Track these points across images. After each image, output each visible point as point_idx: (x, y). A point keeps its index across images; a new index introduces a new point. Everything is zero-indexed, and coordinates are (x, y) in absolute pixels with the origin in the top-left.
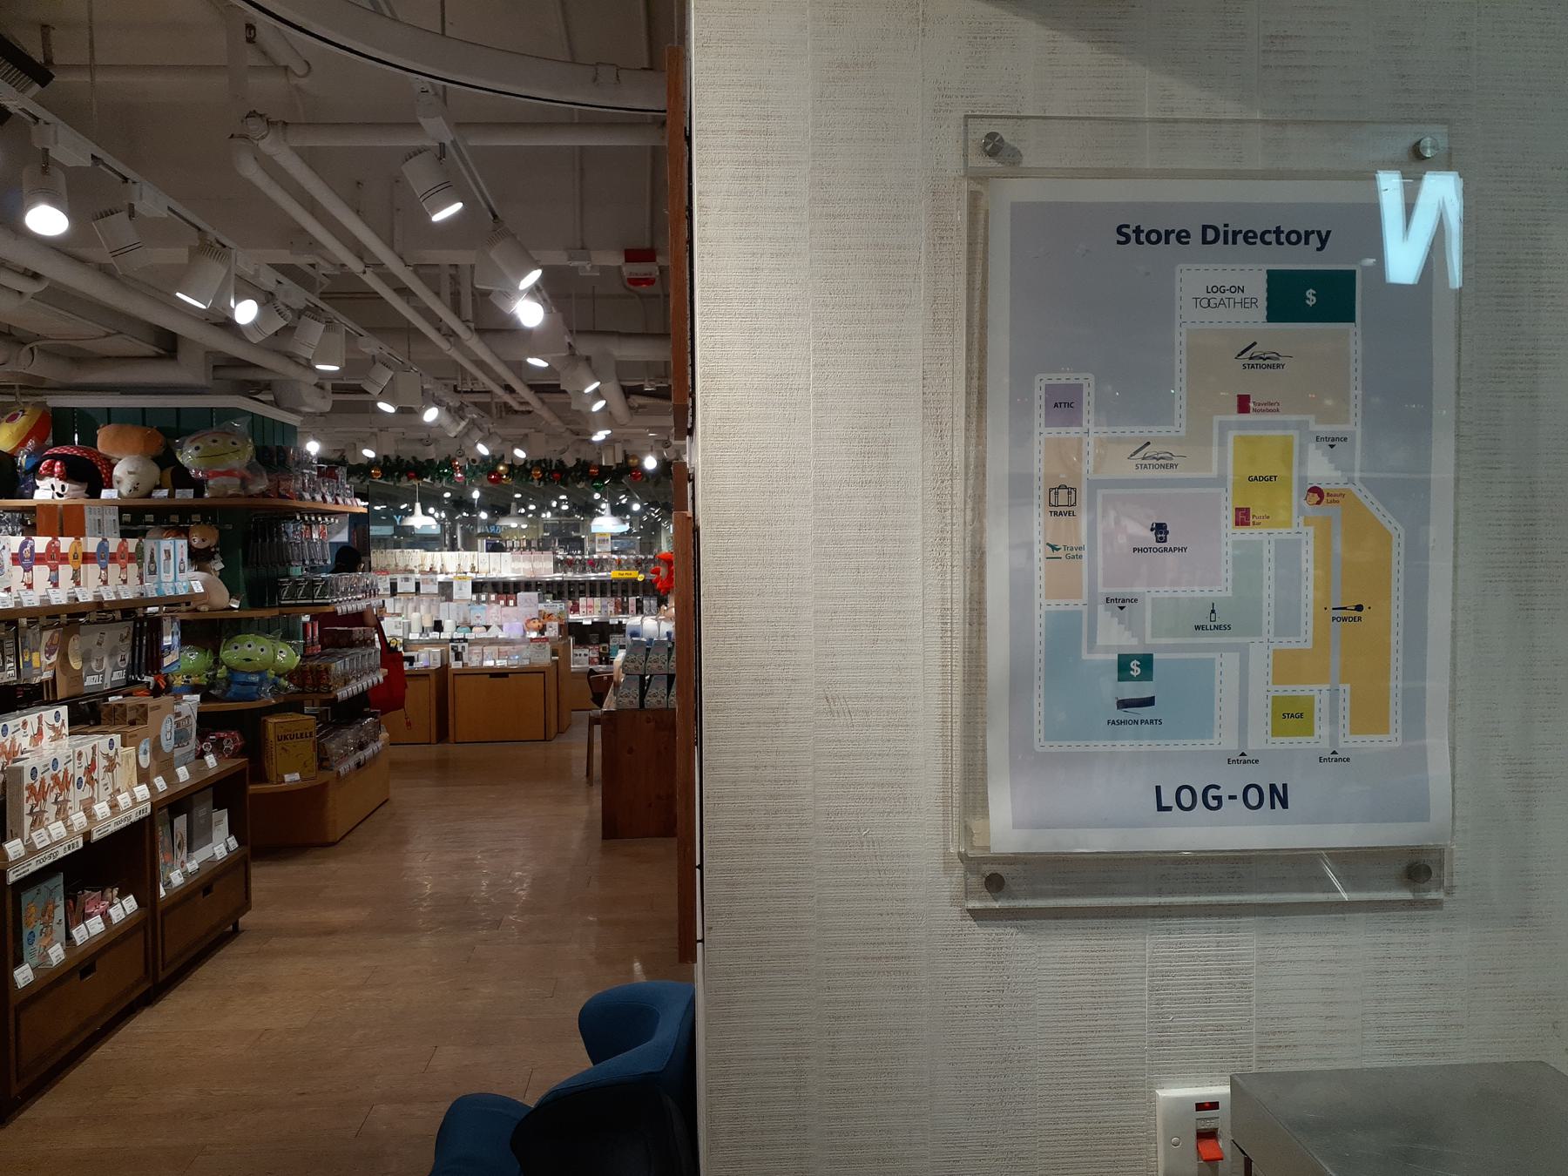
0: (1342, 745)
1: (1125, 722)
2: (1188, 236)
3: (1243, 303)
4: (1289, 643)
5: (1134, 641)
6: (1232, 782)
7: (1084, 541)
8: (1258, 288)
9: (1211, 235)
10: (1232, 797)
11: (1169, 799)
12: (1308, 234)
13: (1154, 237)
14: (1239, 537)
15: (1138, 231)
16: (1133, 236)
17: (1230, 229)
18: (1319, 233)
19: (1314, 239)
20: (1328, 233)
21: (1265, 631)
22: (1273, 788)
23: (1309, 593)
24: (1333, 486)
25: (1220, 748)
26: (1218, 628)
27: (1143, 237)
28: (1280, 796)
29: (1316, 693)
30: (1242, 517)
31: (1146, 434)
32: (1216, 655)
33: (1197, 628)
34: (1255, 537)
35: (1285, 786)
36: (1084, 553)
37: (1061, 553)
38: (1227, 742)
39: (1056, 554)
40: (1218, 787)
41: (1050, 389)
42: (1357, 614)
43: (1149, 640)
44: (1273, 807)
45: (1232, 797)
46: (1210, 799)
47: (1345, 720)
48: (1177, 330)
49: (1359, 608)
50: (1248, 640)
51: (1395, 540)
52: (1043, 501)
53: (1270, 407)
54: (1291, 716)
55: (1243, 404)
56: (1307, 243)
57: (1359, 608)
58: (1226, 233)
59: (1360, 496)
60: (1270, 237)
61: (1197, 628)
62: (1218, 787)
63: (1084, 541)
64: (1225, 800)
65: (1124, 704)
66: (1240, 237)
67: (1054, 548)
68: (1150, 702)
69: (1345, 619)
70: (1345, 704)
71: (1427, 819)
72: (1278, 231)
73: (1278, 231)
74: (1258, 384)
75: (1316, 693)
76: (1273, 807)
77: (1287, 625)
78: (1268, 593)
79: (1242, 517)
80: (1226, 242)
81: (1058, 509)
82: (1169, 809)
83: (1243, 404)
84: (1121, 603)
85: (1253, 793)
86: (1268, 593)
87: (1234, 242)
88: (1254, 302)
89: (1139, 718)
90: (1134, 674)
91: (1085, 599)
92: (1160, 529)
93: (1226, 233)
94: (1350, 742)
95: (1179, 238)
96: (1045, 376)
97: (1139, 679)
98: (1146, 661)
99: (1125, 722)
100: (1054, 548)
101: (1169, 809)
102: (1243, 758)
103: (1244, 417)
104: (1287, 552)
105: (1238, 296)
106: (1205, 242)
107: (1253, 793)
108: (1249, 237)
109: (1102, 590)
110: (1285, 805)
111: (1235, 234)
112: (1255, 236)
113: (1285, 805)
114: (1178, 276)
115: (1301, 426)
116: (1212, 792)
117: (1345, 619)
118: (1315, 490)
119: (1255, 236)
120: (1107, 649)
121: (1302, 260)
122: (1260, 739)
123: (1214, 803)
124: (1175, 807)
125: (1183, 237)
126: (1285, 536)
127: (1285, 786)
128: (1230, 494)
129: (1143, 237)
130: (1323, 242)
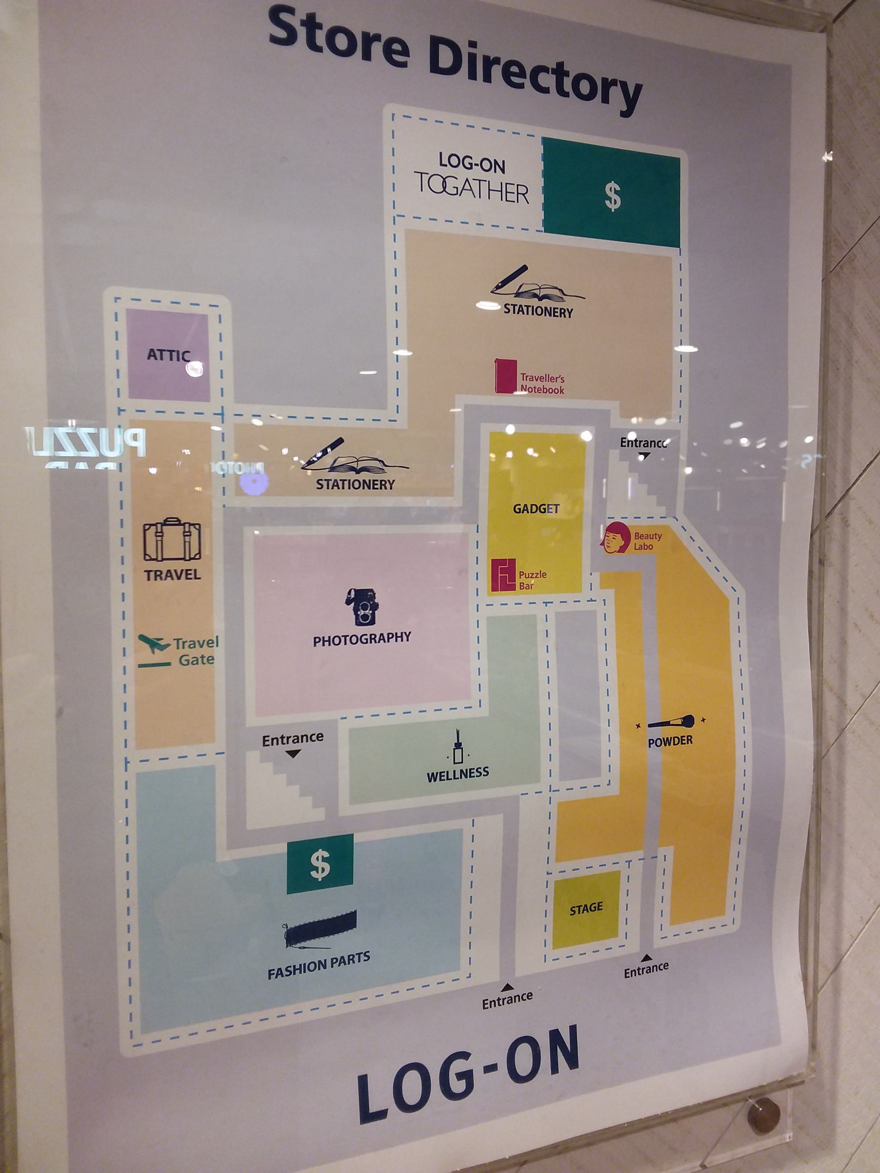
0: (658, 943)
1: (303, 968)
2: (405, 52)
3: (504, 192)
4: (582, 789)
5: (319, 815)
6: (488, 1042)
7: (219, 627)
8: (528, 169)
9: (446, 58)
10: (491, 1068)
11: (381, 1097)
12: (607, 84)
13: (342, 42)
14: (497, 611)
15: (311, 23)
16: (302, 32)
17: (480, 52)
18: (624, 85)
19: (616, 93)
20: (638, 88)
21: (544, 772)
22: (555, 1036)
23: (609, 704)
24: (644, 522)
25: (471, 983)
26: (467, 774)
27: (321, 38)
28: (565, 1048)
29: (622, 866)
30: (504, 575)
31: (335, 423)
32: (464, 824)
33: (432, 777)
34: (525, 610)
35: (573, 1029)
36: (219, 653)
37: (170, 654)
38: (482, 968)
39: (159, 656)
40: (465, 1055)
41: (137, 318)
42: (684, 731)
43: (347, 809)
44: (555, 1069)
45: (491, 1068)
46: (452, 1080)
47: (663, 905)
48: (389, 229)
49: (688, 721)
50: (516, 790)
51: (733, 608)
52: (131, 551)
53: (548, 385)
54: (585, 907)
55: (506, 376)
56: (605, 100)
57: (688, 721)
58: (472, 58)
59: (684, 538)
60: (547, 80)
61: (432, 777)
62: (465, 1055)
63: (219, 627)
64: (479, 1077)
65: (297, 935)
66: (497, 71)
67: (154, 644)
68: (347, 922)
69: (667, 742)
70: (664, 881)
71: (778, 1042)
72: (560, 71)
73: (560, 71)
74: (533, 343)
75: (622, 867)
76: (555, 1069)
77: (580, 763)
78: (549, 704)
79: (504, 575)
80: (472, 76)
81: (164, 566)
82: (382, 1114)
83: (506, 376)
84: (291, 744)
85: (524, 1053)
86: (549, 704)
87: (487, 78)
88: (523, 193)
89: (327, 956)
90: (319, 876)
91: (220, 744)
92: (363, 602)
93: (472, 58)
94: (667, 936)
95: (388, 53)
96: (127, 292)
97: (330, 882)
98: (341, 849)
99: (303, 968)
100: (154, 644)
101: (382, 1114)
102: (509, 994)
103: (505, 399)
104: (575, 630)
105: (496, 178)
106: (435, 68)
107: (524, 1053)
108: (513, 73)
109: (256, 721)
110: (573, 1063)
111: (489, 63)
112: (522, 74)
113: (573, 1063)
114: (387, 125)
115: (598, 420)
116: (458, 1066)
117: (667, 742)
118: (617, 528)
119: (522, 74)
120: (264, 836)
121: (593, 127)
122: (537, 954)
123: (458, 1086)
124: (393, 1109)
125: (396, 52)
126: (571, 607)
127: (573, 1029)
128: (483, 537)
129: (321, 38)
130: (631, 102)
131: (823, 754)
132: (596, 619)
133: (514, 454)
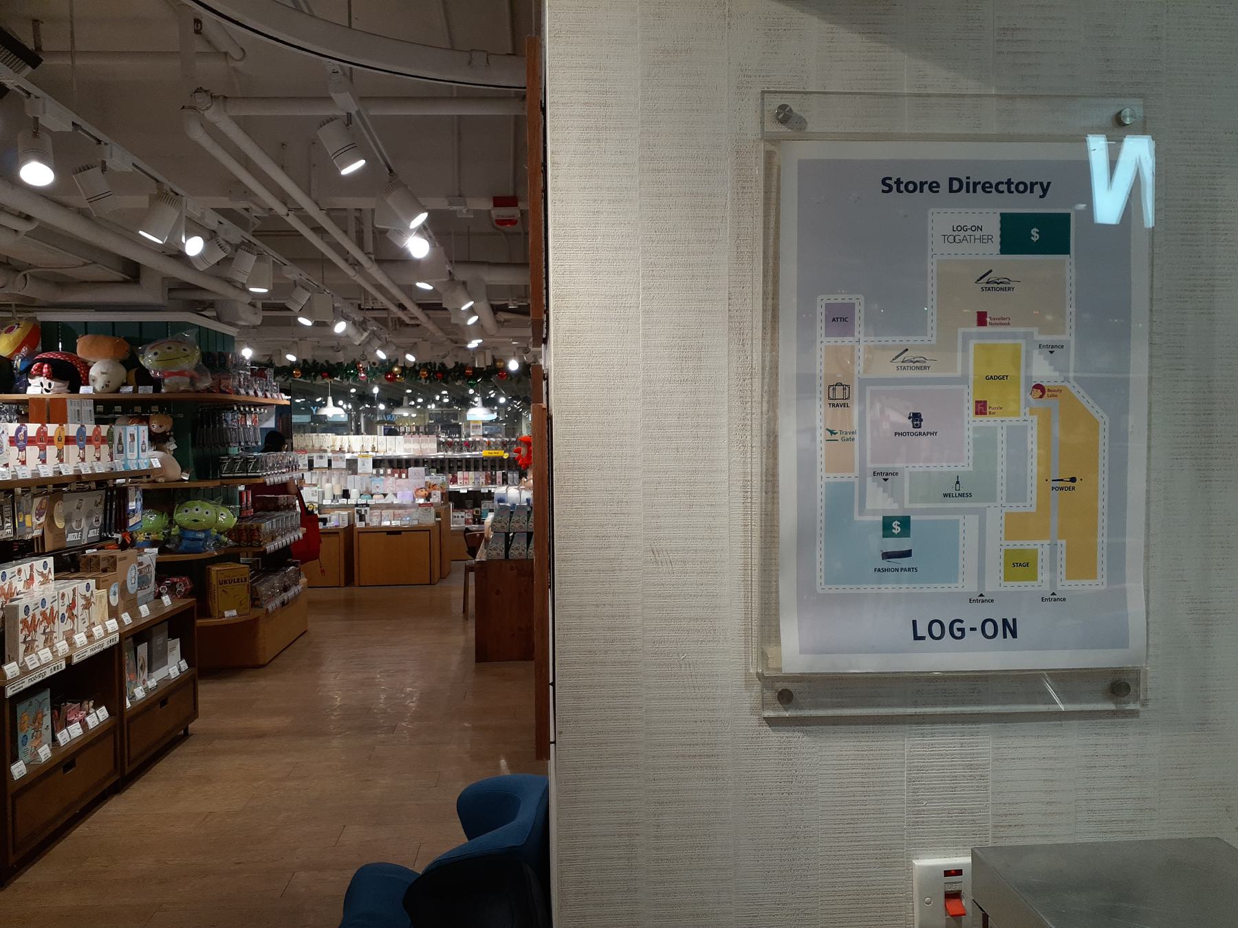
0: (1059, 588)
1: (888, 570)
2: (938, 186)
3: (981, 239)
4: (1018, 508)
5: (896, 506)
6: (972, 617)
7: (856, 427)
8: (993, 228)
9: (956, 185)
10: (972, 629)
11: (923, 631)
12: (1032, 184)
13: (911, 187)
14: (978, 424)
15: (898, 182)
16: (895, 186)
17: (971, 181)
18: (1041, 184)
19: (1037, 188)
20: (1049, 184)
21: (999, 498)
22: (1005, 622)
23: (1033, 468)
24: (1052, 384)
25: (963, 590)
26: (962, 495)
27: (902, 187)
28: (1010, 628)
29: (1039, 547)
30: (981, 408)
31: (905, 343)
32: (960, 517)
33: (945, 495)
34: (991, 424)
35: (1014, 620)
36: (856, 437)
37: (838, 437)
38: (969, 585)
39: (834, 437)
40: (961, 621)
41: (829, 307)
42: (1071, 484)
43: (907, 505)
44: (1005, 637)
45: (972, 629)
46: (956, 630)
47: (1062, 568)
48: (930, 260)
49: (1073, 480)
50: (985, 505)
51: (1101, 426)
52: (824, 396)
53: (1003, 321)
54: (1020, 565)
55: (982, 319)
56: (1032, 191)
57: (1073, 480)
58: (968, 184)
59: (1074, 392)
60: (1003, 187)
61: (945, 495)
62: (961, 621)
63: (856, 427)
64: (967, 631)
65: (887, 556)
66: (979, 187)
67: (832, 432)
68: (908, 554)
69: (1062, 489)
70: (1062, 556)
71: (1127, 647)
72: (1009, 183)
73: (1009, 183)
74: (993, 303)
75: (1039, 547)
76: (1005, 637)
77: (1016, 494)
78: (1001, 468)
79: (981, 408)
80: (968, 191)
81: (835, 402)
82: (923, 638)
83: (982, 319)
84: (885, 476)
85: (989, 626)
86: (1001, 468)
87: (975, 191)
88: (990, 238)
89: (899, 567)
90: (896, 532)
91: (857, 473)
92: (916, 418)
93: (968, 184)
94: (1066, 586)
95: (931, 188)
96: (825, 297)
97: (899, 535)
98: (905, 522)
99: (888, 570)
100: (832, 432)
101: (923, 638)
102: (981, 598)
103: (982, 329)
104: (1016, 436)
105: (978, 234)
106: (951, 191)
107: (989, 626)
108: (986, 187)
109: (870, 465)
110: (1014, 635)
111: (975, 184)
112: (991, 187)
113: (1014, 635)
114: (930, 218)
115: (1027, 336)
116: (957, 625)
117: (1062, 489)
118: (1038, 387)
119: (991, 187)
120: (874, 512)
121: (1028, 205)
122: (995, 583)
123: (958, 634)
124: (928, 637)
125: (934, 187)
126: (1014, 423)
127: (1014, 620)
128: (971, 390)
129: (902, 187)
130: (1045, 191)
131: (421, 200)
132: (299, 186)
133: (250, 346)
